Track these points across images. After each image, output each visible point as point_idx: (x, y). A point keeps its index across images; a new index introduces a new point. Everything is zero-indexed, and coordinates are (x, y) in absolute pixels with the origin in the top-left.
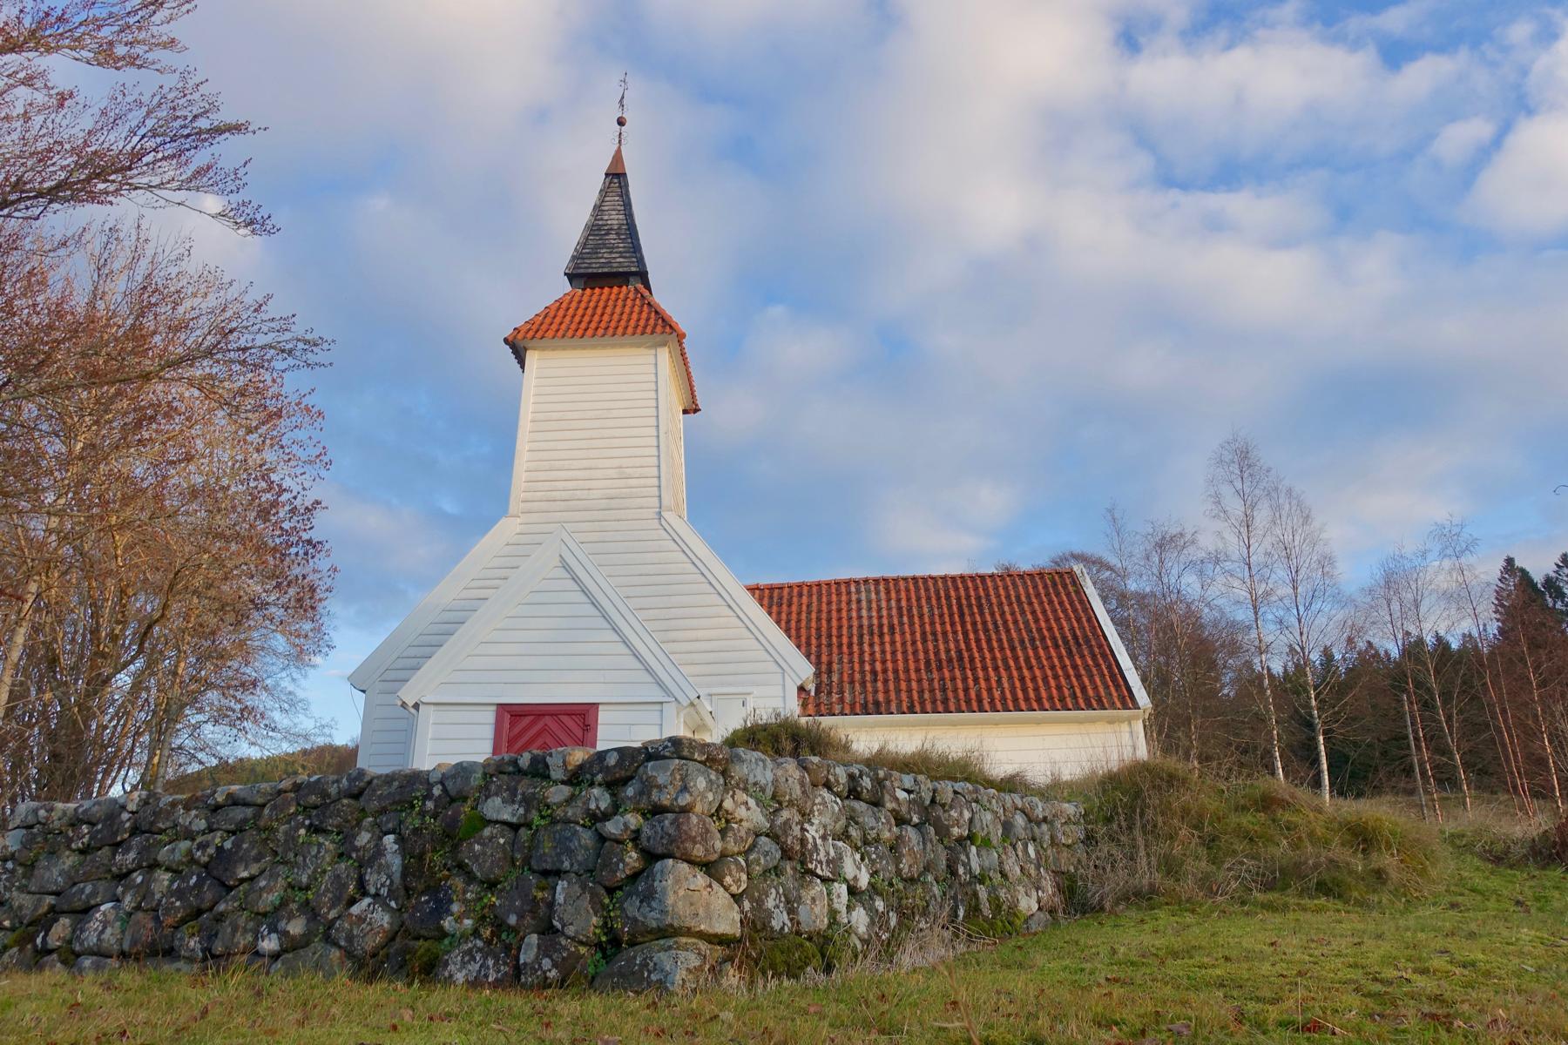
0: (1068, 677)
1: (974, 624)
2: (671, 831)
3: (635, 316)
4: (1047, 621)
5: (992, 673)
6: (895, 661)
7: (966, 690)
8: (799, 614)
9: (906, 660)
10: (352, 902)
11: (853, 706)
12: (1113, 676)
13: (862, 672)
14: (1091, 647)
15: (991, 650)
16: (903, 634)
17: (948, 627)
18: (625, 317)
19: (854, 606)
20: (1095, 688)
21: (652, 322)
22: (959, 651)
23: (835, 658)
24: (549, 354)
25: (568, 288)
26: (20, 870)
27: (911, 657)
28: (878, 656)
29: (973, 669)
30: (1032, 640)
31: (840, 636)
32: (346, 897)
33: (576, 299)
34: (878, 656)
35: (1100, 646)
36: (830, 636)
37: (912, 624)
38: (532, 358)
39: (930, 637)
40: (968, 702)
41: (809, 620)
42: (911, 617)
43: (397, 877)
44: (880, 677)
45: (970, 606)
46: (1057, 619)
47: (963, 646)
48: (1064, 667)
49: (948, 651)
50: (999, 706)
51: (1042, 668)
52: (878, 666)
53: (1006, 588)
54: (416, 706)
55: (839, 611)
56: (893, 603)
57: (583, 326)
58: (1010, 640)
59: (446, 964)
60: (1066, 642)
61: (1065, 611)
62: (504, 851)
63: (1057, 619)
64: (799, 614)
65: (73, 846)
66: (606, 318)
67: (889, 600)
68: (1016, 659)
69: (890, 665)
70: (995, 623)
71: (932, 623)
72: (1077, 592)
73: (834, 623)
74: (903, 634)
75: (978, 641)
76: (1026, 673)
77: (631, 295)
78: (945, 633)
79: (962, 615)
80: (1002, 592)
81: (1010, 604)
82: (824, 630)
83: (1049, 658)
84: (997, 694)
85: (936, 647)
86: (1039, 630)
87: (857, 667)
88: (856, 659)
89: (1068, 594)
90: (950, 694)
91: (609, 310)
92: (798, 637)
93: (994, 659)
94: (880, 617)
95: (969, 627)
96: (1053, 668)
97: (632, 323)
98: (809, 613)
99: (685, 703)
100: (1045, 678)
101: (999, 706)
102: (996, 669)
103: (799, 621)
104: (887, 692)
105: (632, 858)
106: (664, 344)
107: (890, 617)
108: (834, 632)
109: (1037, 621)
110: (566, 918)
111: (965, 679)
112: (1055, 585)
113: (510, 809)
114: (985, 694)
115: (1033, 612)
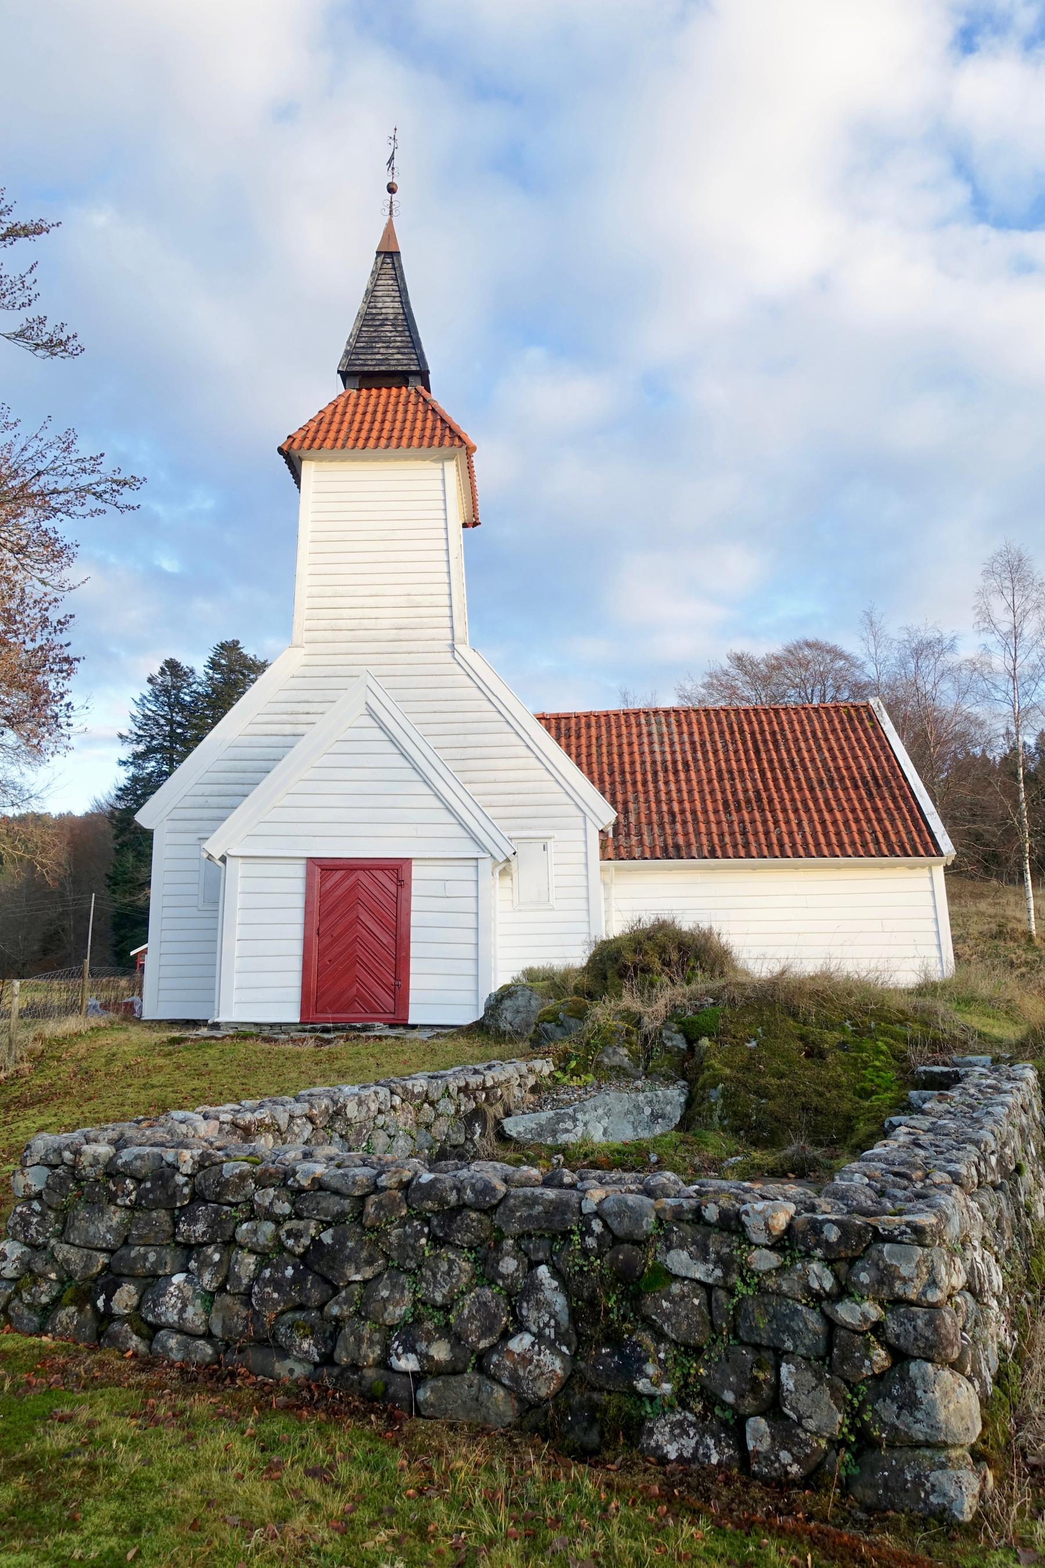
0: (869, 821)
1: (770, 761)
2: (928, 1333)
3: (419, 424)
4: (845, 759)
5: (792, 816)
6: (692, 801)
7: (767, 833)
8: (589, 746)
9: (703, 801)
10: (506, 1336)
11: (652, 849)
12: (914, 820)
13: (660, 812)
14: (891, 788)
15: (790, 790)
16: (698, 771)
17: (745, 766)
18: (408, 425)
19: (645, 740)
20: (898, 833)
21: (438, 432)
22: (757, 792)
23: (631, 797)
24: (326, 465)
25: (342, 389)
26: (52, 1215)
27: (708, 797)
28: (674, 795)
29: (773, 811)
30: (831, 780)
31: (633, 773)
32: (499, 1329)
33: (352, 401)
34: (674, 795)
35: (901, 788)
36: (623, 772)
37: (706, 761)
38: (308, 469)
39: (726, 776)
40: (770, 846)
41: (600, 755)
42: (705, 753)
43: (564, 1318)
44: (678, 818)
45: (765, 741)
46: (855, 758)
47: (761, 786)
48: (864, 810)
49: (746, 791)
50: (801, 852)
51: (842, 810)
52: (676, 807)
53: (801, 722)
54: (223, 859)
55: (630, 744)
56: (686, 737)
57: (364, 434)
58: (808, 779)
59: (651, 1432)
60: (866, 784)
61: (862, 749)
62: (701, 1313)
63: (855, 758)
64: (589, 746)
65: (119, 1201)
66: (387, 425)
67: (681, 734)
68: (816, 801)
69: (687, 805)
70: (792, 761)
71: (728, 760)
72: (874, 728)
73: (626, 758)
74: (698, 771)
75: (775, 780)
76: (827, 816)
77: (413, 399)
78: (741, 771)
79: (757, 752)
80: (797, 727)
81: (806, 740)
82: (616, 765)
83: (849, 800)
84: (798, 838)
85: (733, 786)
86: (838, 769)
87: (653, 806)
88: (652, 798)
89: (865, 730)
90: (751, 838)
91: (389, 416)
92: (602, 781)
93: (793, 800)
94: (673, 753)
95: (766, 765)
96: (853, 810)
97: (417, 433)
98: (599, 746)
99: (501, 858)
100: (846, 822)
101: (801, 852)
102: (796, 811)
103: (589, 755)
104: (686, 834)
105: (880, 1356)
106: (451, 458)
107: (683, 752)
108: (627, 768)
109: (834, 759)
110: (802, 1408)
111: (765, 822)
112: (850, 719)
113: (703, 1268)
114: (786, 839)
115: (830, 750)
